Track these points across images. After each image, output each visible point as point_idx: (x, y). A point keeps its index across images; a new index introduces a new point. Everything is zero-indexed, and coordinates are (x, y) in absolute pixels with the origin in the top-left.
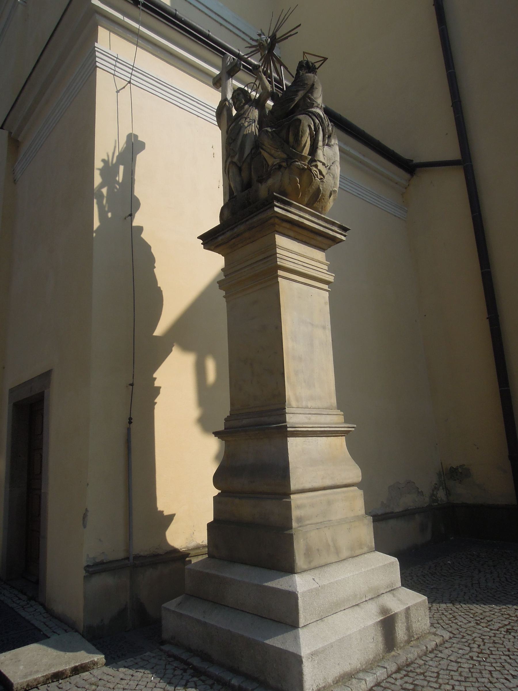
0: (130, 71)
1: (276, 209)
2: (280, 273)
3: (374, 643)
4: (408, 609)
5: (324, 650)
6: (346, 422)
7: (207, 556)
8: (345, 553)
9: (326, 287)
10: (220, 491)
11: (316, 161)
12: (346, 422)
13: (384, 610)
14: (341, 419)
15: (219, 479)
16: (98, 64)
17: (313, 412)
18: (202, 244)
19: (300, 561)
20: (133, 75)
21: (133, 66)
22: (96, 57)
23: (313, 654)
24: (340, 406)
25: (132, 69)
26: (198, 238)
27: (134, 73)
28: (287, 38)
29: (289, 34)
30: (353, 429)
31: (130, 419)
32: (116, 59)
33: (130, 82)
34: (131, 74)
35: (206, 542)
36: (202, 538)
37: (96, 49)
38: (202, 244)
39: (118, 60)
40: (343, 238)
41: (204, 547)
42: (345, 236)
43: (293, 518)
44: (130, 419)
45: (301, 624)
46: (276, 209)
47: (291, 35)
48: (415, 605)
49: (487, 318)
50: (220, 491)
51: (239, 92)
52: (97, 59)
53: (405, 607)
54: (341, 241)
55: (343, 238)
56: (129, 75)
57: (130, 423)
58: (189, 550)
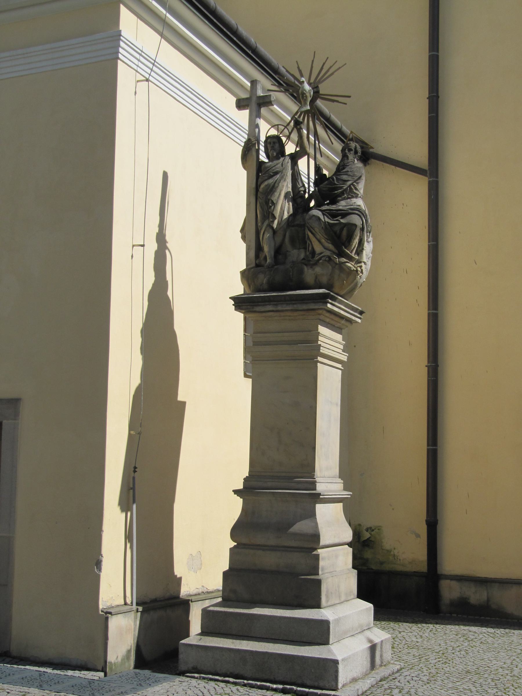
0: (151, 66)
1: (329, 305)
2: (319, 359)
3: (364, 662)
4: (382, 641)
5: (349, 657)
6: (345, 489)
7: (220, 600)
8: (343, 598)
9: (340, 366)
10: (236, 544)
11: (361, 262)
12: (345, 489)
13: (370, 641)
14: (341, 486)
15: (235, 532)
16: (120, 56)
17: (329, 481)
18: (233, 305)
19: (324, 601)
20: (151, 72)
21: (155, 61)
22: (119, 46)
23: (342, 660)
24: (341, 476)
25: (154, 64)
26: (231, 298)
27: (155, 69)
28: (333, 101)
29: (325, 77)
30: (350, 496)
31: (135, 468)
32: (140, 52)
33: (147, 80)
34: (152, 70)
35: (221, 588)
36: (216, 583)
37: (122, 38)
38: (233, 305)
39: (143, 54)
40: (359, 321)
41: (219, 591)
42: (360, 318)
43: (320, 567)
44: (135, 468)
45: (330, 643)
46: (329, 305)
47: (337, 101)
48: (386, 639)
49: (426, 366)
50: (236, 544)
51: (275, 140)
52: (121, 50)
53: (380, 640)
54: (357, 322)
55: (359, 321)
56: (149, 71)
57: (135, 471)
58: (191, 596)
